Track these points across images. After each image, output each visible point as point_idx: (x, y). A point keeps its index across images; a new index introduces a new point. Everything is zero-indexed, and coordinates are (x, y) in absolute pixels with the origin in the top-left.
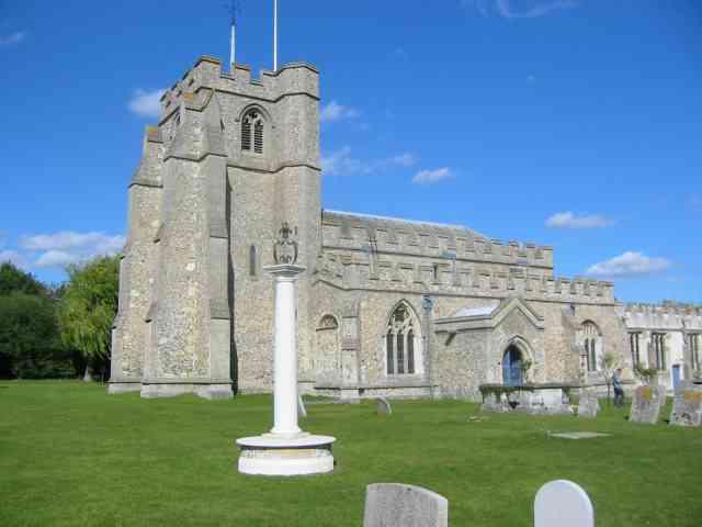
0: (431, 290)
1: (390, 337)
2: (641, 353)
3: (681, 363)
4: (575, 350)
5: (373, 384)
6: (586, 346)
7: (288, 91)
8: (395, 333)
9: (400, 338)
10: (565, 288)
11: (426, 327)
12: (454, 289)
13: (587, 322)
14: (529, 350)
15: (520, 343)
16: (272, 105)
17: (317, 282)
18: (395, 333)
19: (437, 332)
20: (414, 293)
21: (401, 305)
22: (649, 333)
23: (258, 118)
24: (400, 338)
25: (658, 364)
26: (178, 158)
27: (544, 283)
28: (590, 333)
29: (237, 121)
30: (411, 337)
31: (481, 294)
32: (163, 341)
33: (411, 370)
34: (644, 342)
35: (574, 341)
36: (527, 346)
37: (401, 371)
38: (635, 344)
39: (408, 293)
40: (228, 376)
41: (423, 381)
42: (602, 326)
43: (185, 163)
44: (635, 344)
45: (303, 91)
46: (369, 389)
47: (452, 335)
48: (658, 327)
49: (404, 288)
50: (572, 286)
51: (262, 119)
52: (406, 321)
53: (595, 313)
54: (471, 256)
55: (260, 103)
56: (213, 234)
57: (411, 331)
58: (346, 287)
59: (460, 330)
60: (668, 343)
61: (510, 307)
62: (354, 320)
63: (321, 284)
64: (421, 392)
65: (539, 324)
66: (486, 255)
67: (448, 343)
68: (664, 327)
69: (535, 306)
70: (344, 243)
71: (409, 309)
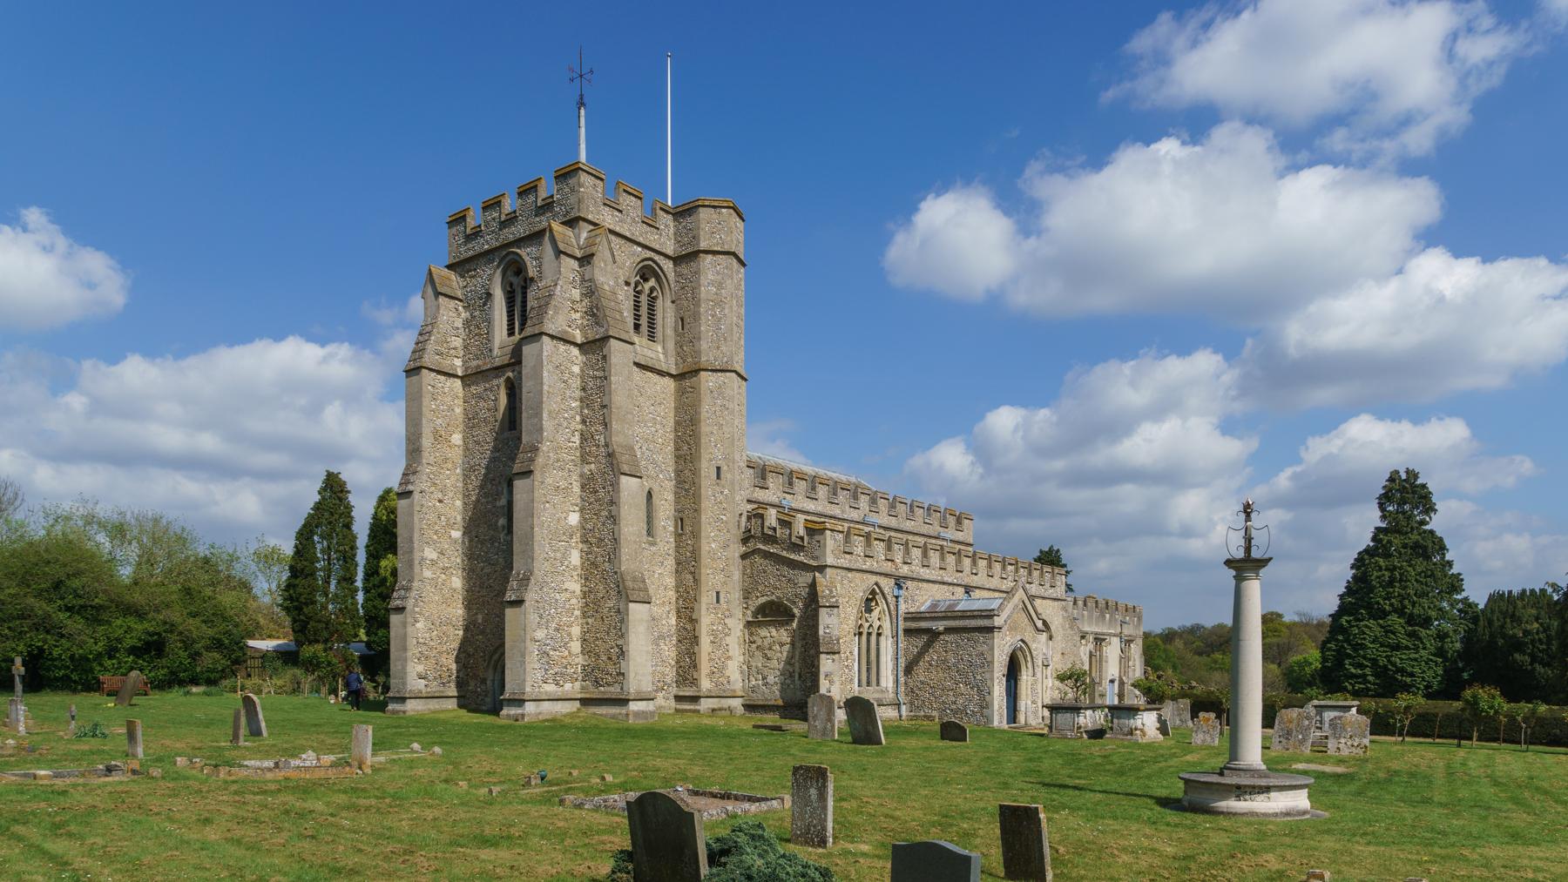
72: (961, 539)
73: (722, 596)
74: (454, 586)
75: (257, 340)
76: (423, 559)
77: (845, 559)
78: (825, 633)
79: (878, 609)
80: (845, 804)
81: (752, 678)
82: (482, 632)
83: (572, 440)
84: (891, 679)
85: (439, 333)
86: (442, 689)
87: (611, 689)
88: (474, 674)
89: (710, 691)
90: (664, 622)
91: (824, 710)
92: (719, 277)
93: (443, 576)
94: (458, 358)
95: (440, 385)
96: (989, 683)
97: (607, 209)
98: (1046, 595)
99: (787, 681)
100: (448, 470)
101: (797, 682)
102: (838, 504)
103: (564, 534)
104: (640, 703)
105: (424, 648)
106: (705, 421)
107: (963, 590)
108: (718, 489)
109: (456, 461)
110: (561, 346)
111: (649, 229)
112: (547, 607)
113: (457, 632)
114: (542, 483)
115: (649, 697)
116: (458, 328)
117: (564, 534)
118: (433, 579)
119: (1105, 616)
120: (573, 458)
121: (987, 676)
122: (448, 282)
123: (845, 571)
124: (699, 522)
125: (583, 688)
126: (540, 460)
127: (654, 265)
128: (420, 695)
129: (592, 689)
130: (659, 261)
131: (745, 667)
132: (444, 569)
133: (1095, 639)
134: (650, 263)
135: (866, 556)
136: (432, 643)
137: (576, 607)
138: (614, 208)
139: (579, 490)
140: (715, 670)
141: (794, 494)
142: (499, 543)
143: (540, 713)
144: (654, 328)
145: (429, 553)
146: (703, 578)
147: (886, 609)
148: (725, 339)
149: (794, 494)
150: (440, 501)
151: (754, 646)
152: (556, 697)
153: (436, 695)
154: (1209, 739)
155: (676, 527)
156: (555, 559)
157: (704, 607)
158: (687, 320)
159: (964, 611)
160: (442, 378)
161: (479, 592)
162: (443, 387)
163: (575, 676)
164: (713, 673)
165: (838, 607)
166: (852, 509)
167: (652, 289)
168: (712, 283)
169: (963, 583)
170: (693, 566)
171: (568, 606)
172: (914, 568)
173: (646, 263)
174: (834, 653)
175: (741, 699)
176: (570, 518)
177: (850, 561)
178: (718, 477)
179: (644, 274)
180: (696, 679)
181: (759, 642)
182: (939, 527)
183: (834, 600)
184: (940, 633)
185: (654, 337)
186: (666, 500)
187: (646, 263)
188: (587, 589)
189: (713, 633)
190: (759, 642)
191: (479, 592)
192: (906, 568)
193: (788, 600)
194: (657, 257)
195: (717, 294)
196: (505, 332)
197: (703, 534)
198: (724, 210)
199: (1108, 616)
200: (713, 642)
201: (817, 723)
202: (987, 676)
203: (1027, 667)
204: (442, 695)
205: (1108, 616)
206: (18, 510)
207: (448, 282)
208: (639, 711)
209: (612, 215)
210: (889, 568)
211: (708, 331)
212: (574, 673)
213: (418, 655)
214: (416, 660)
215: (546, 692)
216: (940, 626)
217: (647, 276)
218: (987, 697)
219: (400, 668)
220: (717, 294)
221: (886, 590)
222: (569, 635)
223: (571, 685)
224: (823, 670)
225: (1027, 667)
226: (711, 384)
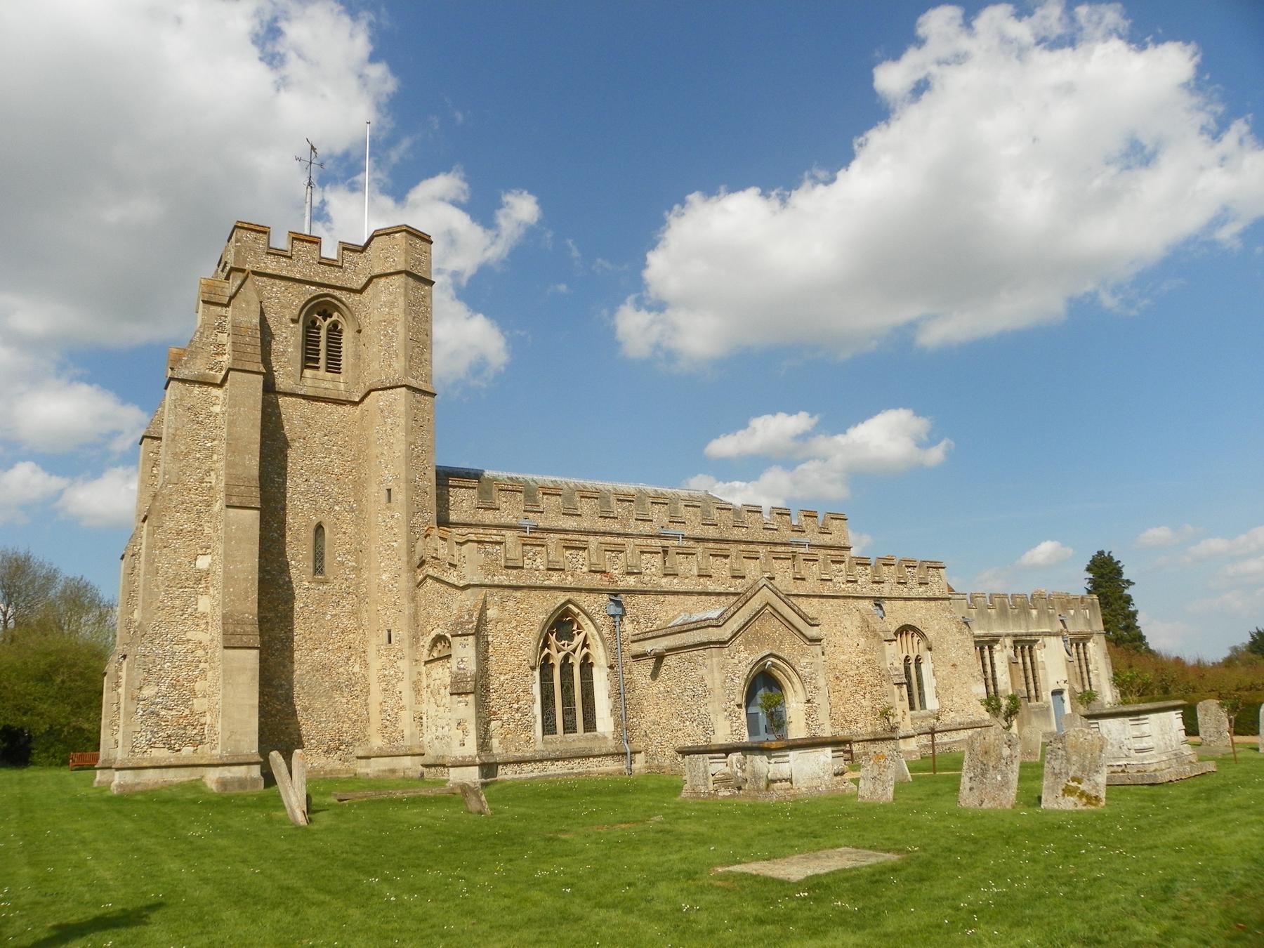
0: (622, 585)
1: (545, 667)
2: (998, 674)
3: (1066, 687)
4: (883, 676)
5: (513, 754)
6: (907, 669)
7: (377, 271)
8: (557, 659)
9: (566, 667)
10: (864, 577)
11: (614, 651)
12: (664, 581)
13: (905, 630)
14: (795, 679)
15: (774, 665)
16: (357, 297)
17: (425, 578)
18: (557, 659)
19: (636, 657)
20: (590, 591)
21: (567, 612)
22: (1008, 642)
23: (333, 318)
24: (566, 667)
25: (1028, 691)
26: (184, 381)
27: (826, 565)
28: (912, 646)
29: (294, 321)
30: (587, 665)
31: (711, 588)
32: (148, 692)
33: (590, 724)
34: (1002, 655)
35: (884, 659)
36: (790, 672)
37: (570, 728)
38: (988, 661)
39: (579, 590)
40: (255, 750)
41: (611, 745)
42: (930, 635)
43: (197, 390)
44: (988, 661)
45: (399, 268)
46: (506, 764)
47: (660, 658)
48: (1023, 631)
49: (570, 581)
50: (876, 570)
51: (341, 319)
52: (578, 639)
53: (915, 614)
54: (711, 532)
55: (337, 293)
56: (235, 501)
57: (586, 657)
58: (462, 583)
59: (668, 650)
60: (1040, 654)
61: (755, 604)
62: (471, 638)
63: (429, 581)
64: (610, 766)
65: (813, 632)
66: (736, 531)
67: (655, 675)
68: (1033, 630)
69: (806, 606)
70: (489, 517)
71: (582, 619)
72: (830, 543)
77: (507, 575)
78: (459, 669)
89: (381, 749)
90: (341, 670)
98: (912, 595)
106: (375, 442)
107: (872, 602)
108: (389, 513)
119: (1029, 613)
130: (339, 296)
133: (1014, 642)
135: (549, 569)
138: (280, 255)
143: (138, 784)
156: (173, 607)
166: (639, 522)
178: (389, 500)
182: (789, 532)
185: (339, 369)
189: (384, 678)
194: (331, 291)
195: (389, 313)
200: (385, 690)
206: (878, 608)
211: (380, 351)
217: (329, 312)
226: (381, 403)
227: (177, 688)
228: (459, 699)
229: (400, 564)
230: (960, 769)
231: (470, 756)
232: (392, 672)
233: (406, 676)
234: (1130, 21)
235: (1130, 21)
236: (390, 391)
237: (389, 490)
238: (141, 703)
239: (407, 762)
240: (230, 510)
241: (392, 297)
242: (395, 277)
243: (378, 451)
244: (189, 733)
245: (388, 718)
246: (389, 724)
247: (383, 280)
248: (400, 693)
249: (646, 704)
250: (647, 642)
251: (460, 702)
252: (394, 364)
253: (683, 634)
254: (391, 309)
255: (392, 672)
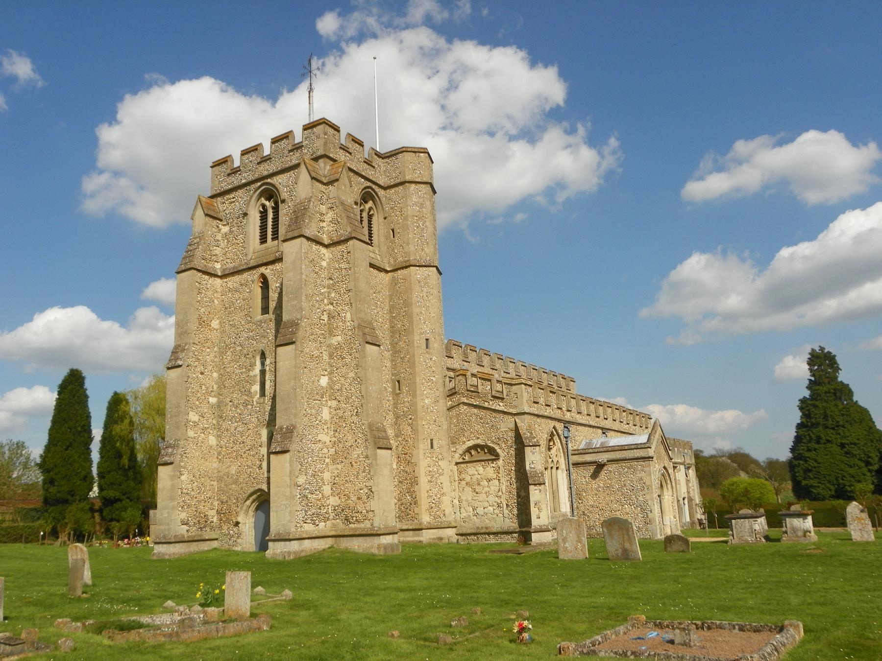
47: (600, 467)
59: (608, 461)
73: (435, 443)
74: (210, 443)
75: (540, 65)
76: (188, 421)
79: (555, 447)
80: (7, 584)
81: (462, 510)
82: (236, 482)
83: (321, 318)
84: (568, 504)
85: (205, 243)
86: (200, 533)
87: (362, 525)
88: (228, 519)
89: (429, 523)
91: (573, 532)
92: (421, 200)
93: (203, 435)
94: (218, 262)
95: (204, 282)
96: (650, 503)
97: (342, 151)
99: (495, 511)
100: (208, 348)
101: (506, 512)
102: (496, 370)
103: (317, 394)
104: (388, 537)
105: (187, 497)
109: (214, 341)
110: (314, 246)
111: (368, 166)
112: (306, 456)
113: (212, 483)
114: (302, 352)
115: (394, 531)
116: (218, 241)
117: (317, 394)
118: (195, 438)
120: (323, 332)
121: (648, 497)
122: (212, 207)
123: (536, 418)
124: (415, 383)
125: (334, 525)
126: (300, 334)
127: (372, 192)
128: (183, 540)
129: (342, 526)
131: (456, 502)
132: (204, 429)
134: (370, 190)
136: (193, 493)
137: (327, 455)
139: (327, 358)
140: (433, 505)
141: (469, 362)
142: (252, 405)
143: (302, 551)
144: (372, 237)
145: (193, 417)
146: (420, 428)
147: (561, 447)
148: (427, 244)
149: (469, 362)
150: (202, 373)
151: (463, 483)
152: (314, 536)
153: (196, 538)
154: (866, 536)
155: (394, 388)
157: (421, 452)
158: (397, 231)
159: (622, 446)
160: (207, 277)
161: (232, 448)
162: (206, 284)
163: (327, 516)
164: (432, 508)
165: (539, 446)
167: (370, 209)
168: (415, 204)
169: (601, 426)
170: (411, 419)
171: (321, 455)
172: (573, 414)
173: (367, 190)
174: (540, 484)
175: (454, 529)
176: (321, 381)
177: (538, 409)
179: (365, 198)
180: (417, 514)
181: (468, 479)
183: (535, 440)
184: (604, 465)
186: (386, 367)
187: (367, 190)
188: (336, 439)
190: (468, 479)
191: (232, 448)
192: (568, 414)
193: (493, 442)
194: (374, 187)
195: (419, 211)
196: (258, 241)
197: (418, 392)
198: (422, 155)
199: (676, 449)
201: (567, 545)
202: (648, 497)
203: (667, 489)
204: (199, 538)
205: (676, 449)
207: (212, 207)
208: (388, 544)
209: (345, 156)
210: (559, 415)
211: (414, 238)
212: (326, 513)
213: (182, 504)
214: (180, 509)
215: (306, 531)
216: (603, 458)
218: (650, 514)
219: (166, 515)
220: (419, 211)
221: (560, 432)
222: (322, 479)
223: (324, 524)
224: (533, 499)
225: (667, 489)
226: (419, 276)
227: (316, 477)
228: (536, 488)
229: (438, 393)
230: (719, 528)
231: (544, 525)
232: (435, 469)
233: (445, 472)
234: (539, 62)
235: (539, 62)
236: (425, 269)
237: (427, 340)
238: (299, 488)
239: (451, 532)
240: (367, 345)
241: (421, 200)
242: (423, 186)
243: (417, 310)
244: (322, 511)
245: (433, 501)
246: (435, 506)
247: (413, 186)
248: (441, 484)
249: (584, 494)
250: (587, 455)
251: (536, 490)
252: (426, 249)
253: (624, 452)
254: (421, 208)
255: (435, 469)
